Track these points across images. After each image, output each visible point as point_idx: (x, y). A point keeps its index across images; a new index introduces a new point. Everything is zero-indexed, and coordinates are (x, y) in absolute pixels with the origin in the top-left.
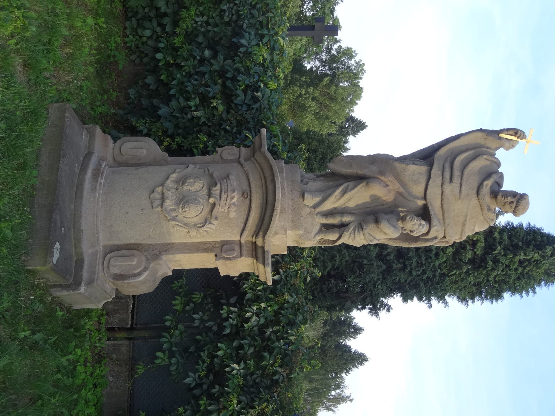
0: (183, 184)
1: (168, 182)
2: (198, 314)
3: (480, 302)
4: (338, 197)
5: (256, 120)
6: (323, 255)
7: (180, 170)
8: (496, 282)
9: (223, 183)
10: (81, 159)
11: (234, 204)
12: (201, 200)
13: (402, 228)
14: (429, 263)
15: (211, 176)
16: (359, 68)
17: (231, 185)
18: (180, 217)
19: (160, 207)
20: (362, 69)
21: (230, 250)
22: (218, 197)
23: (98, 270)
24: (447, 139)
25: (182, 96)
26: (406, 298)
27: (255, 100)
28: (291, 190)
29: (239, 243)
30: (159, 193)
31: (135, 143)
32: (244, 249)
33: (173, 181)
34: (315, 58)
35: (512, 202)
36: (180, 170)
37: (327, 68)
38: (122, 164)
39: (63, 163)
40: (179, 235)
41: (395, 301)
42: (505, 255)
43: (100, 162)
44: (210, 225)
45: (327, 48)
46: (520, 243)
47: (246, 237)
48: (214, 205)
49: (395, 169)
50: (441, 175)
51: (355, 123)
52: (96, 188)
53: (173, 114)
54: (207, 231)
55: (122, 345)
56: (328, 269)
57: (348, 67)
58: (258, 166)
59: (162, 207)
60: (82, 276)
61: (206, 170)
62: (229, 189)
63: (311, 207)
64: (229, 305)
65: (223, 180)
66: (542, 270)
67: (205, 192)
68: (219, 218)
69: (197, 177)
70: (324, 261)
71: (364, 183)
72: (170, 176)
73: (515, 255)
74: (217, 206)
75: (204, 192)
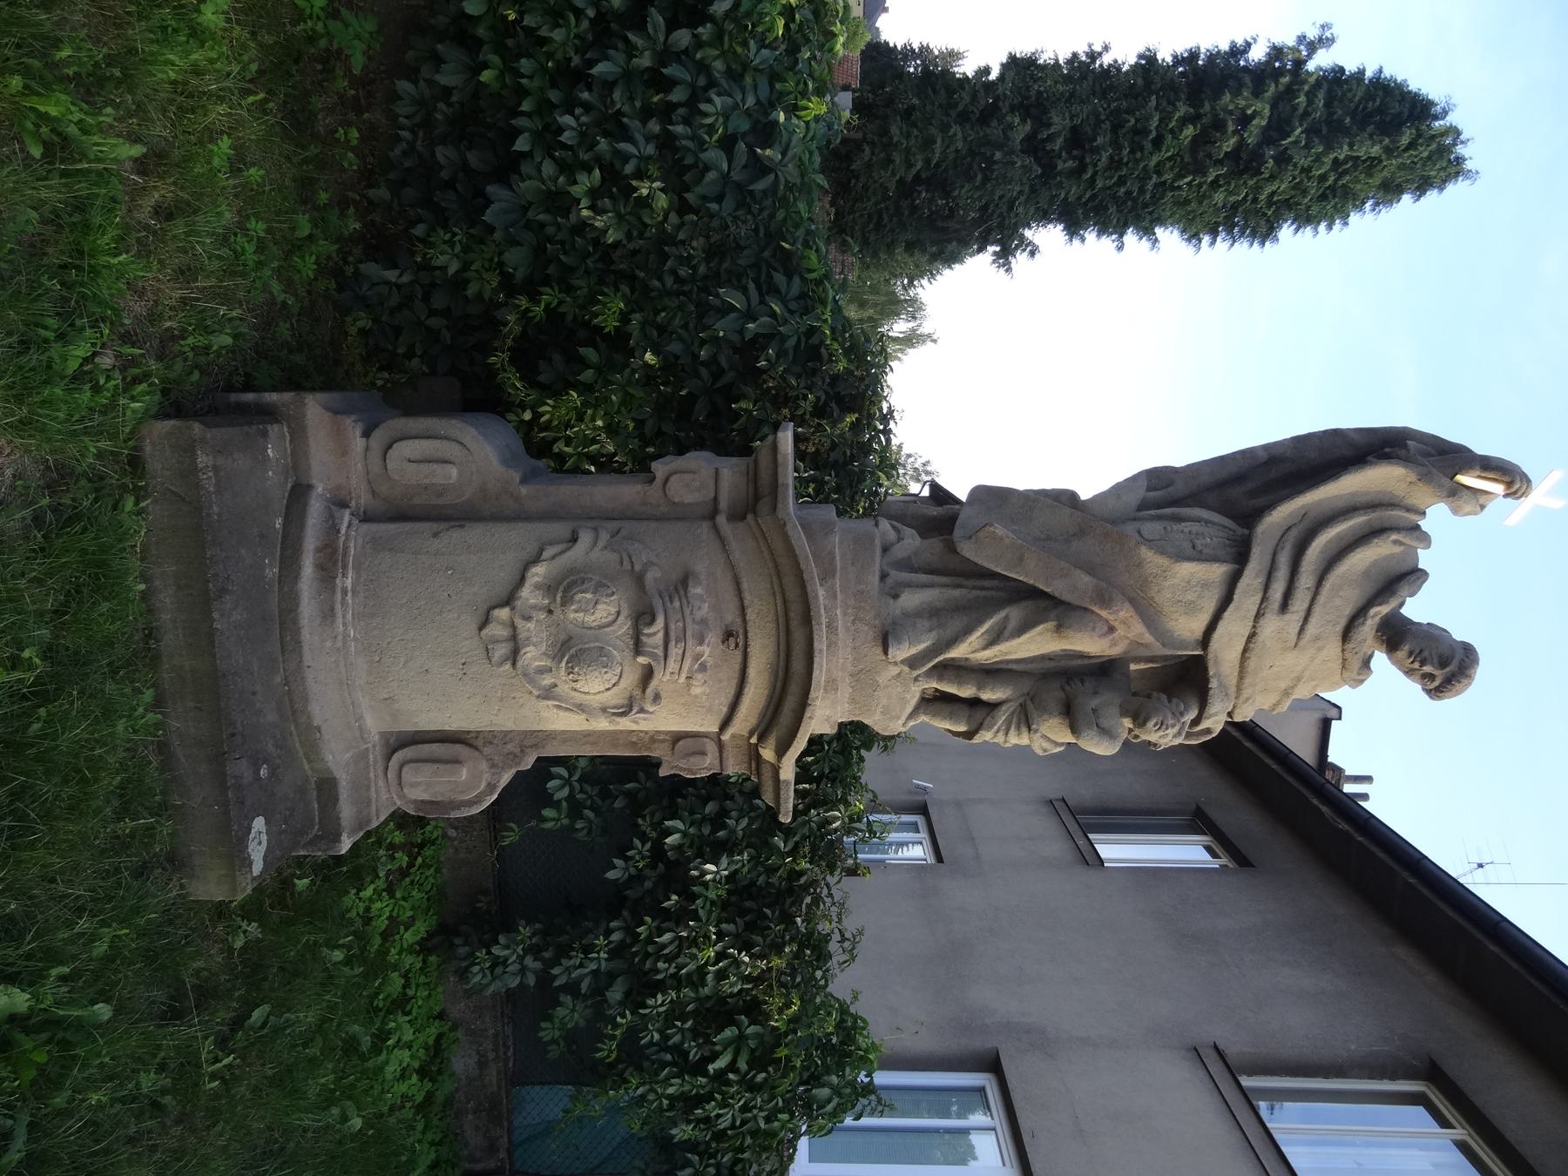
0: (565, 602)
1: (525, 592)
3: (1227, 244)
4: (976, 645)
6: (908, 136)
8: (1270, 203)
9: (670, 612)
10: (279, 523)
13: (1130, 730)
14: (1137, 161)
18: (564, 688)
19: (508, 666)
21: (695, 753)
22: (660, 652)
24: (1300, 442)
25: (552, 157)
26: (1074, 229)
27: (760, 168)
28: (853, 622)
30: (503, 623)
33: (537, 586)
35: (1431, 677)
38: (401, 512)
41: (1048, 236)
42: (1308, 146)
43: (332, 516)
46: (1348, 120)
49: (1139, 565)
50: (1261, 587)
52: (332, 609)
56: (914, 171)
58: (766, 553)
59: (514, 664)
60: (338, 818)
62: (689, 633)
63: (902, 662)
66: (1376, 180)
67: (624, 627)
68: (663, 695)
70: (908, 150)
71: (1051, 625)
72: (529, 574)
73: (1329, 148)
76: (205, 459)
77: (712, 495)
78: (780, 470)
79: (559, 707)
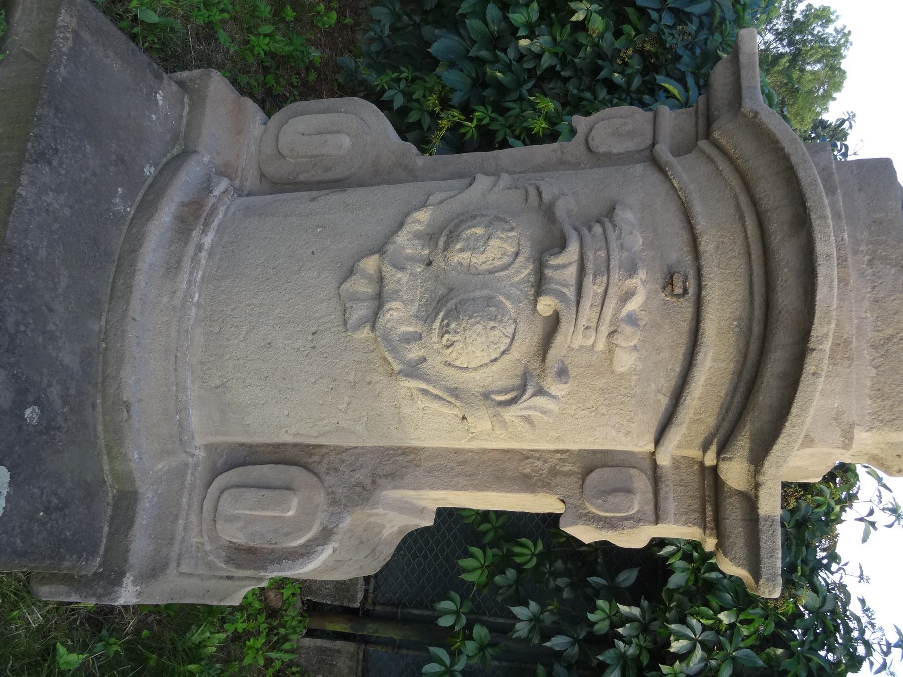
0: (447, 246)
1: (402, 238)
2: (527, 605)
5: (698, 51)
7: (444, 195)
10: (149, 170)
11: (632, 320)
12: (508, 304)
15: (548, 213)
16: (840, 39)
17: (622, 247)
18: (434, 364)
19: (367, 329)
20: (847, 41)
22: (571, 293)
23: (186, 528)
28: (871, 263)
29: (647, 464)
30: (370, 278)
31: (322, 118)
32: (669, 490)
33: (417, 235)
34: (766, 28)
36: (444, 195)
37: (785, 42)
39: (32, 183)
40: (432, 426)
43: (209, 180)
44: (539, 400)
45: (787, 11)
47: (679, 447)
48: (554, 324)
51: (827, 130)
52: (179, 262)
53: (472, 53)
54: (528, 420)
55: (339, 651)
57: (822, 39)
61: (532, 191)
62: (614, 263)
64: (617, 595)
65: (590, 229)
67: (524, 272)
68: (573, 371)
69: (497, 220)
72: (410, 219)
74: (566, 327)
75: (518, 271)
76: (68, 19)
77: (649, 142)
78: (744, 73)
79: (425, 392)
